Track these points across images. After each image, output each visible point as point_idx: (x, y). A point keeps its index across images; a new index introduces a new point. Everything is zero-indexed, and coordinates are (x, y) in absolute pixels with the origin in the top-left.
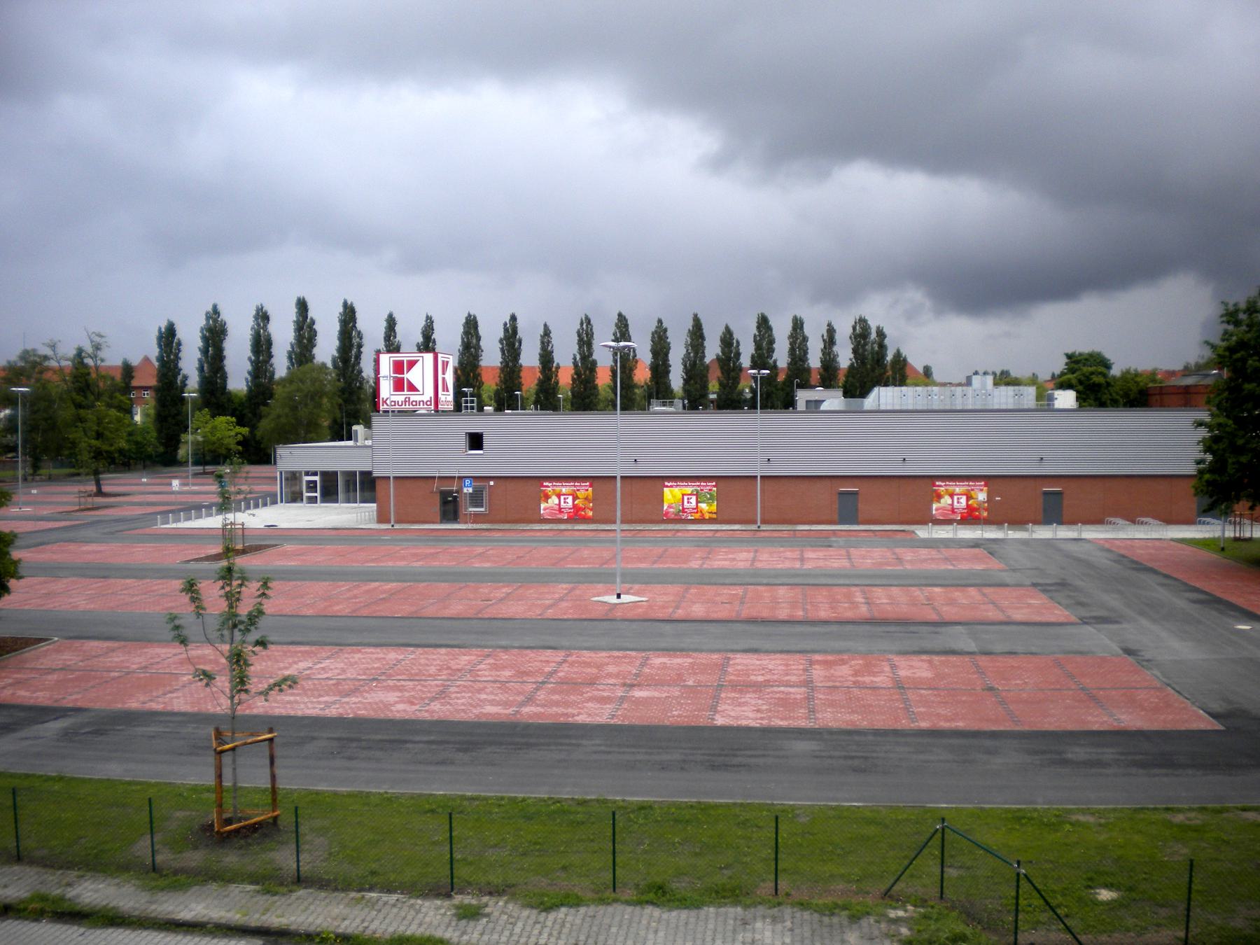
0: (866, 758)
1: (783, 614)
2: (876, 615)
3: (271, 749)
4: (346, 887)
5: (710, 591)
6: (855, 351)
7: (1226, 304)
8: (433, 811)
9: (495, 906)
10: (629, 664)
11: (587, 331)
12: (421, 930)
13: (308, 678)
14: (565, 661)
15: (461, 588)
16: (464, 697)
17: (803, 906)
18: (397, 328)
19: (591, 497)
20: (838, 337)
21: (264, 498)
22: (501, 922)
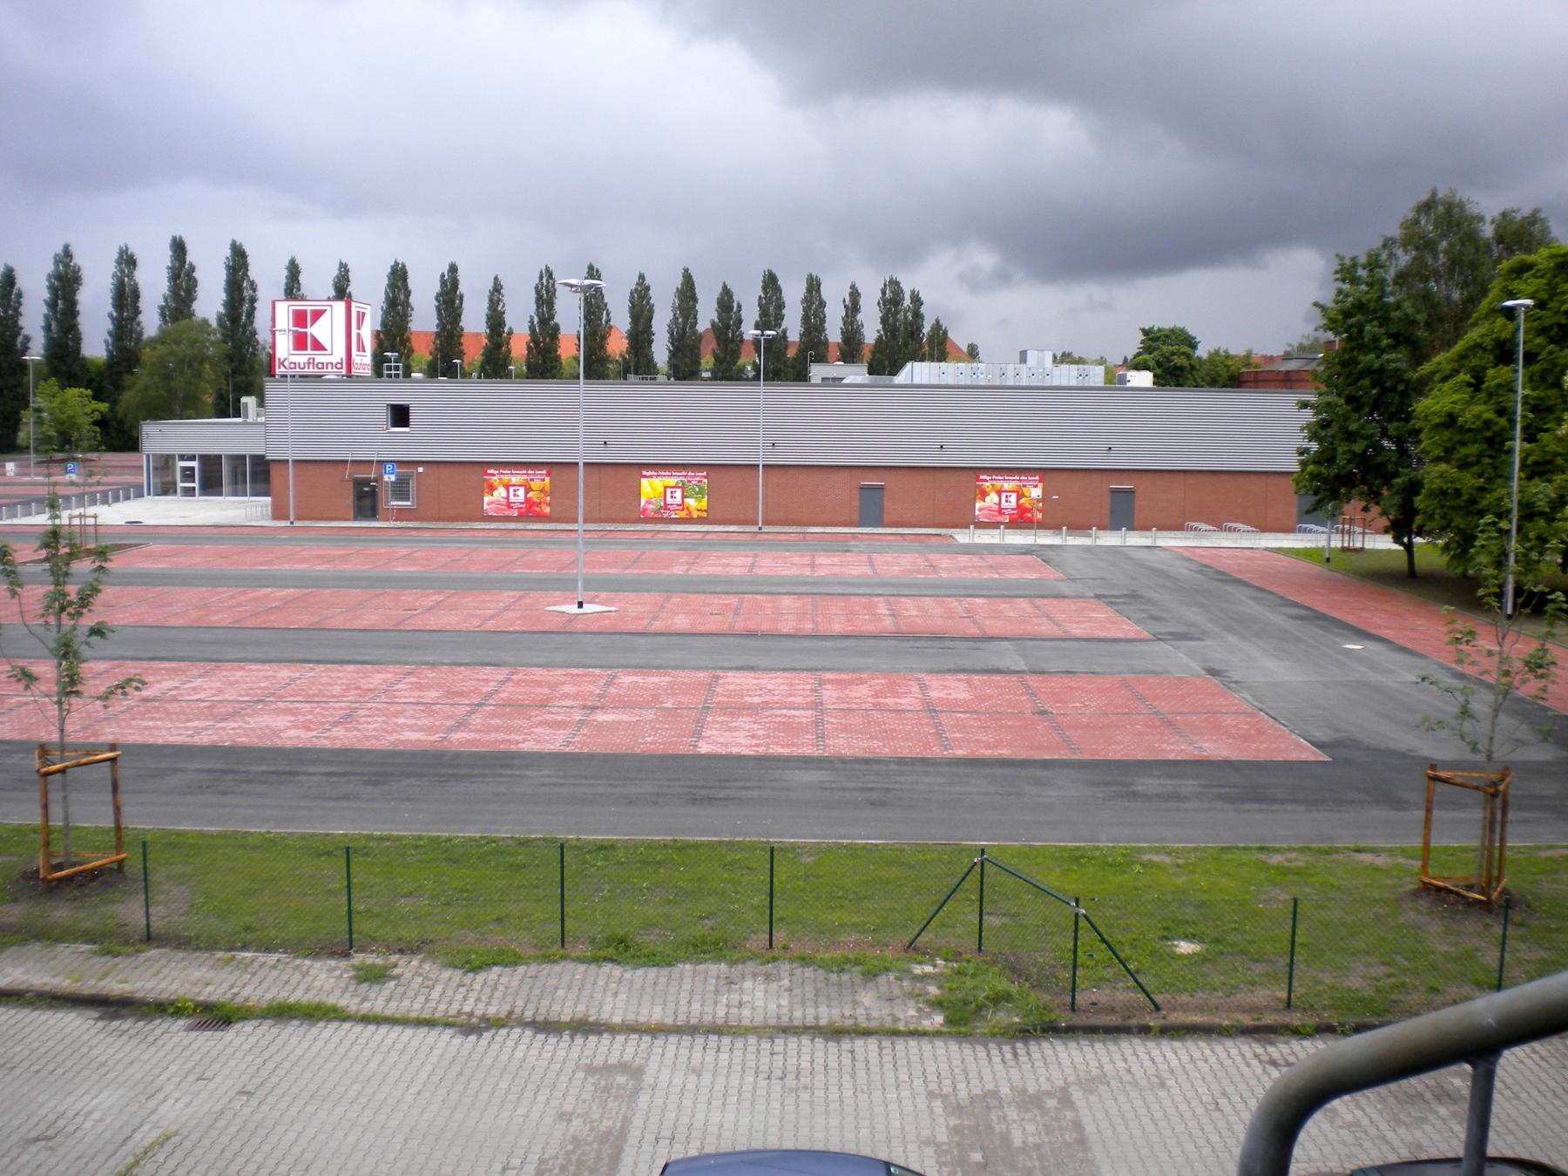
0: (887, 790)
1: (787, 626)
2: (904, 628)
3: (114, 771)
4: (211, 945)
5: (697, 600)
6: (884, 321)
7: (1342, 258)
8: (329, 854)
9: (406, 967)
10: (591, 683)
11: (547, 287)
12: (310, 996)
13: (174, 699)
14: (508, 680)
15: (376, 596)
16: (376, 722)
17: (804, 961)
18: (302, 278)
19: (548, 488)
20: (862, 302)
21: (127, 491)
22: (414, 986)
